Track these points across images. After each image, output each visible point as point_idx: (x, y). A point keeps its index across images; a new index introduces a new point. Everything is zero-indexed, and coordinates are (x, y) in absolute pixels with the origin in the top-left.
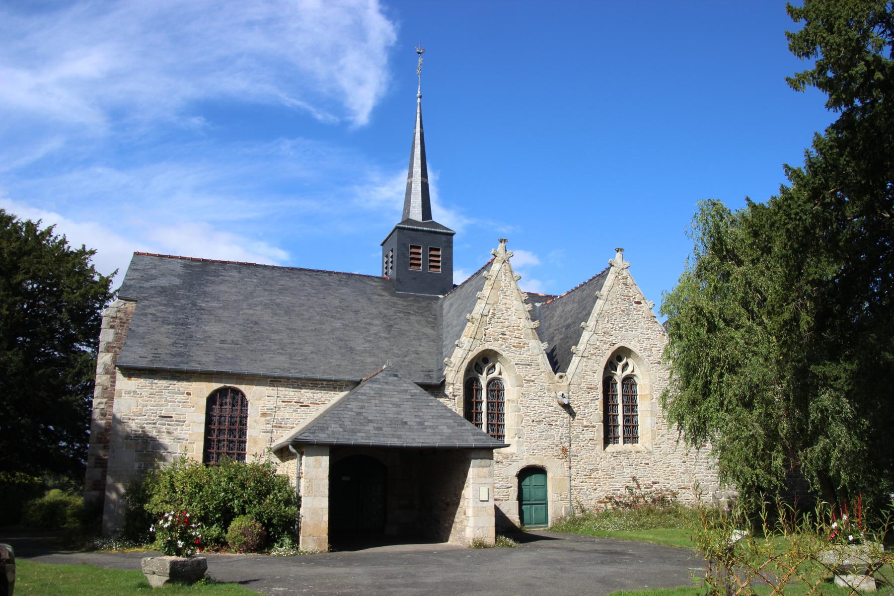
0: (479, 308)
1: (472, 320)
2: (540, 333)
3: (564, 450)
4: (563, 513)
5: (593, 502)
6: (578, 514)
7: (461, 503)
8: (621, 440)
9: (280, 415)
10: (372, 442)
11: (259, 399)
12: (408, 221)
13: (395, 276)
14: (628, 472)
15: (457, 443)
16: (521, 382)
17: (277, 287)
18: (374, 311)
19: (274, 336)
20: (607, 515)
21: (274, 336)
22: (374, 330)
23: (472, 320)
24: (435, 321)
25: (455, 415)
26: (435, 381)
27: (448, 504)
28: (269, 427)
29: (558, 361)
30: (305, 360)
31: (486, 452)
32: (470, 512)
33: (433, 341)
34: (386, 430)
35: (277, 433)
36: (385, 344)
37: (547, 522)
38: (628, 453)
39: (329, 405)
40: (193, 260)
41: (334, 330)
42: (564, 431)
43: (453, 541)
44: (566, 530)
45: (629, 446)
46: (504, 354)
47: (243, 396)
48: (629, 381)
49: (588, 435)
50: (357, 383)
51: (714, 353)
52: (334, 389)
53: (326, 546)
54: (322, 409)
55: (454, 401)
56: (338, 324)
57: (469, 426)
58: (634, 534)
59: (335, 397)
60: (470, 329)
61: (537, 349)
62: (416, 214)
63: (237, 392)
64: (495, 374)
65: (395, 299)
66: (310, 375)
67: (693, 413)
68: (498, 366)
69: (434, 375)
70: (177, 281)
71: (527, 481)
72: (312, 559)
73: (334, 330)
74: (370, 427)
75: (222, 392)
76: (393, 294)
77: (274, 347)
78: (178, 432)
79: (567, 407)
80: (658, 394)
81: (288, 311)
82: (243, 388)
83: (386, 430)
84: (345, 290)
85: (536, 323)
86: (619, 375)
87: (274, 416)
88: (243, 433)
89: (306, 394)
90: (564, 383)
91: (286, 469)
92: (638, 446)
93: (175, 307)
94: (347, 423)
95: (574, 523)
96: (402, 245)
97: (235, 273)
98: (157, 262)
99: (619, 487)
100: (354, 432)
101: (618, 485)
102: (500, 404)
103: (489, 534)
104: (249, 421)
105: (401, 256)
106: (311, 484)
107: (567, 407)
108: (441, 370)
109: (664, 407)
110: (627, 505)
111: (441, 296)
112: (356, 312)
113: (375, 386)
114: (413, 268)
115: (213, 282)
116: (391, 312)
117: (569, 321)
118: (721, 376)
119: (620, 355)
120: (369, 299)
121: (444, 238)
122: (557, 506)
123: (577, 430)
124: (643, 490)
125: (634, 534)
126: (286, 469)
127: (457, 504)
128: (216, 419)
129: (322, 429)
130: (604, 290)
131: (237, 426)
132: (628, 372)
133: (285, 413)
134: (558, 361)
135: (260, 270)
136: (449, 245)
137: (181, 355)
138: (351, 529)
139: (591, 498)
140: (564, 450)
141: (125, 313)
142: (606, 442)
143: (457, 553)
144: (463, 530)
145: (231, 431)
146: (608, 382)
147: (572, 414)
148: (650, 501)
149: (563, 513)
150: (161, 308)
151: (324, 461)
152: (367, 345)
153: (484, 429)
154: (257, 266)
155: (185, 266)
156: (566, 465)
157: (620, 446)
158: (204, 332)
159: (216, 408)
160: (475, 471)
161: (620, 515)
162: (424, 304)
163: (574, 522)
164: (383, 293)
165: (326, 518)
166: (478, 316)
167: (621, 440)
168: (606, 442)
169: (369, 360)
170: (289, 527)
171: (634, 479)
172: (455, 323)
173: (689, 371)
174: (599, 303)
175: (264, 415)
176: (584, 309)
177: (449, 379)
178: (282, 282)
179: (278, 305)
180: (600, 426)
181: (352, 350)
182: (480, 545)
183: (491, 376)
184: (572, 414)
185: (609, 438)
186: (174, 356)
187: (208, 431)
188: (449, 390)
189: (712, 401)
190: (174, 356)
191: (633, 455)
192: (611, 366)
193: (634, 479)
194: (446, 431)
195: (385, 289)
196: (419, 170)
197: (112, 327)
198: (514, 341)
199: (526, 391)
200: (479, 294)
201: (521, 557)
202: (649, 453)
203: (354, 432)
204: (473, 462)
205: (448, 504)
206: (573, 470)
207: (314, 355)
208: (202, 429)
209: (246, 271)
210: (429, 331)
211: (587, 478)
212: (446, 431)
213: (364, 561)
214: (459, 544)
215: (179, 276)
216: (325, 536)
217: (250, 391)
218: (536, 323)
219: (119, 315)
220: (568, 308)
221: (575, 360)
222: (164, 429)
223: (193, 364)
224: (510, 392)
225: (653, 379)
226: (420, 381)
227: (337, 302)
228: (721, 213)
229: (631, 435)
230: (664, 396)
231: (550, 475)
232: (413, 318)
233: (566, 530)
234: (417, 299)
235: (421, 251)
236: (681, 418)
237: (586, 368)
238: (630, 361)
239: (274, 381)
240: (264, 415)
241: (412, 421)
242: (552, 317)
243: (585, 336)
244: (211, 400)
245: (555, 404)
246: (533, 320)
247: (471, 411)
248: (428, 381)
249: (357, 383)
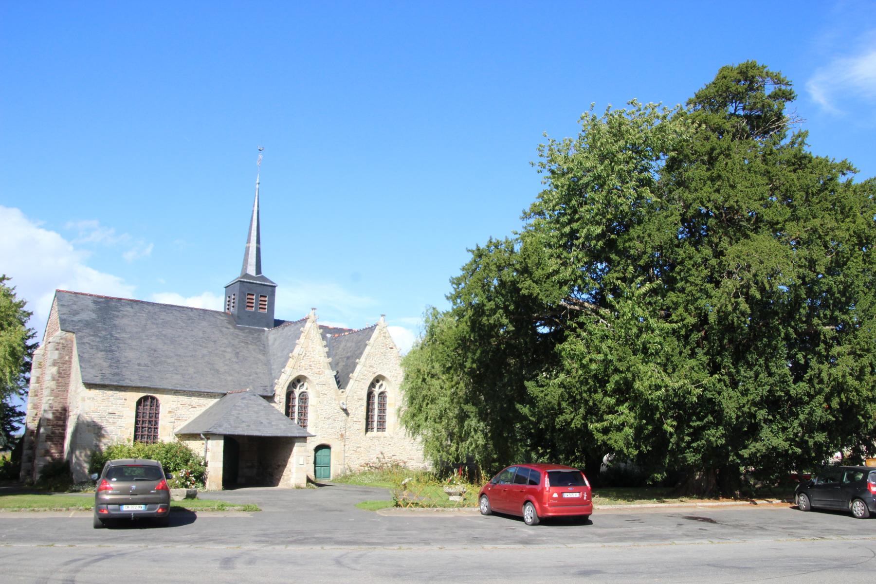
0: (297, 350)
1: (292, 357)
2: (333, 366)
3: (342, 435)
4: (339, 472)
5: (357, 466)
6: (348, 473)
7: (288, 466)
8: (375, 429)
9: (179, 412)
10: (246, 433)
11: (166, 402)
12: (246, 275)
13: (236, 313)
14: (378, 449)
15: (289, 435)
16: (318, 394)
17: (161, 321)
18: (226, 341)
19: (169, 361)
20: (365, 473)
21: (169, 361)
22: (228, 356)
23: (292, 357)
24: (264, 349)
25: (279, 412)
26: (269, 394)
27: (279, 466)
28: (173, 420)
29: (341, 382)
30: (191, 378)
31: (304, 439)
32: (293, 470)
33: (265, 365)
34: (253, 427)
35: (177, 423)
36: (236, 366)
37: (329, 477)
38: (378, 438)
39: (208, 407)
40: (99, 297)
41: (203, 356)
42: (342, 424)
43: (282, 485)
44: (341, 482)
45: (380, 433)
46: (310, 378)
47: (157, 401)
48: (382, 395)
49: (357, 426)
50: (225, 394)
51: (424, 393)
52: (211, 397)
53: (221, 487)
54: (204, 409)
55: (280, 404)
56: (205, 351)
57: (289, 419)
58: (379, 484)
59: (213, 402)
60: (291, 362)
61: (330, 374)
62: (252, 271)
63: (153, 398)
64: (304, 389)
65: (237, 332)
66: (198, 390)
67: (414, 419)
68: (306, 384)
69: (268, 389)
70: (94, 316)
71: (319, 452)
72: (214, 493)
73: (203, 356)
74: (244, 425)
75: (145, 398)
76: (235, 327)
77: (171, 369)
78: (120, 422)
79: (345, 410)
80: (397, 407)
81: (173, 341)
82: (157, 396)
83: (253, 427)
84: (204, 324)
85: (330, 360)
86: (377, 391)
87: (176, 415)
88: (156, 423)
89: (195, 400)
90: (344, 396)
91: (195, 446)
92: (386, 433)
93: (100, 337)
94: (232, 423)
95: (346, 478)
96: (242, 294)
97: (129, 309)
98: (75, 299)
99: (373, 458)
100: (236, 427)
101: (372, 456)
102: (306, 407)
103: (304, 483)
104: (160, 416)
105: (241, 300)
106: (213, 455)
107: (345, 410)
108: (272, 386)
109: (399, 416)
110: (376, 468)
111: (266, 329)
112: (215, 341)
113: (245, 401)
114: (248, 309)
115: (118, 317)
116: (236, 342)
117: (349, 354)
118: (427, 404)
119: (377, 380)
120: (221, 331)
121: (270, 289)
122: (336, 468)
123: (350, 424)
124: (387, 460)
125: (379, 484)
126: (195, 446)
127: (285, 466)
128: (141, 415)
129: (220, 426)
130: (372, 340)
131: (153, 419)
132: (382, 390)
133: (182, 412)
134: (341, 382)
135: (145, 305)
136: (273, 294)
137: (117, 374)
138: (231, 481)
139: (356, 464)
140: (342, 435)
141: (66, 340)
142: (367, 431)
143: (283, 491)
144: (289, 479)
145: (150, 422)
146: (370, 395)
147: (348, 414)
148: (390, 465)
149: (339, 472)
150: (92, 338)
151: (221, 443)
152: (226, 368)
153: (296, 421)
154: (142, 302)
155: (95, 302)
156: (342, 444)
157: (374, 433)
158: (126, 357)
159: (141, 407)
160: (297, 448)
161: (372, 474)
162: (256, 335)
163: (346, 477)
164: (230, 326)
165: (221, 473)
166: (296, 355)
167: (375, 429)
168: (367, 431)
169: (229, 378)
170: (201, 478)
171: (382, 453)
172: (279, 354)
173: (412, 399)
174: (368, 348)
175: (170, 412)
176: (359, 348)
177: (277, 393)
178: (162, 317)
179: (165, 336)
180: (364, 421)
181: (217, 371)
182: (298, 487)
183: (302, 390)
184: (348, 414)
185: (368, 428)
186: (114, 375)
187: (137, 422)
188: (277, 399)
189: (422, 416)
190: (114, 375)
191: (382, 439)
192: (373, 385)
193: (382, 453)
194: (283, 427)
195: (229, 323)
196: (255, 238)
197: (57, 349)
198: (317, 370)
199: (321, 395)
200: (297, 341)
201: (320, 492)
202: (392, 438)
203: (236, 427)
204: (296, 444)
205: (279, 466)
206: (347, 447)
207: (196, 375)
208: (133, 421)
209: (137, 307)
210: (261, 357)
211: (355, 451)
212: (283, 427)
213: (240, 494)
214: (286, 487)
215: (93, 311)
216: (221, 482)
217: (161, 398)
218: (330, 360)
219: (62, 341)
220: (349, 345)
221: (351, 382)
222: (111, 420)
223: (127, 381)
224: (312, 401)
225: (396, 398)
226: (261, 393)
227: (201, 334)
228: (435, 314)
229: (382, 427)
230: (399, 410)
231: (332, 449)
232: (250, 346)
233: (341, 482)
234: (251, 332)
235: (254, 297)
236: (406, 422)
237: (358, 386)
238: (384, 383)
239: (176, 392)
240: (170, 412)
241: (265, 422)
242: (338, 348)
243: (358, 368)
244: (139, 403)
245: (338, 408)
246: (328, 357)
247: (288, 412)
248: (265, 394)
249: (225, 394)
